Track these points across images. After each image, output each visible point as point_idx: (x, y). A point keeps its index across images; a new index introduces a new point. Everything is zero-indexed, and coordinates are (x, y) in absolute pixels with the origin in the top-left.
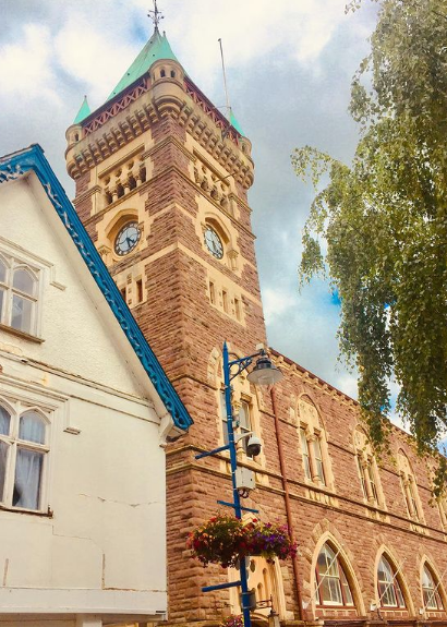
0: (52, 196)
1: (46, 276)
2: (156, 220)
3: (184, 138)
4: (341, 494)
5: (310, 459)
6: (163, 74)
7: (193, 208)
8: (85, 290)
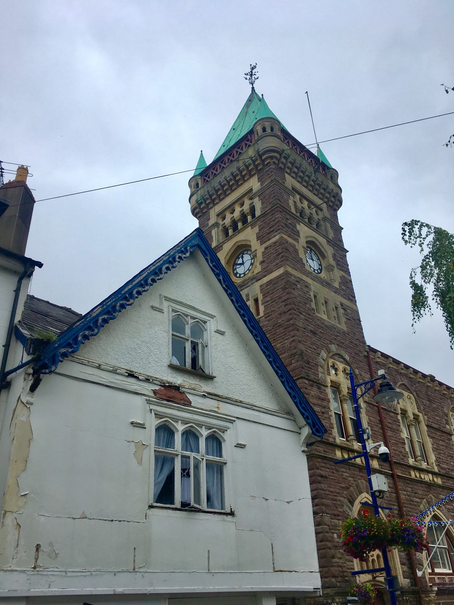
0: (211, 265)
1: (212, 326)
2: (266, 248)
3: (284, 179)
4: (443, 472)
5: (411, 441)
6: (264, 130)
7: (296, 234)
8: (238, 332)
